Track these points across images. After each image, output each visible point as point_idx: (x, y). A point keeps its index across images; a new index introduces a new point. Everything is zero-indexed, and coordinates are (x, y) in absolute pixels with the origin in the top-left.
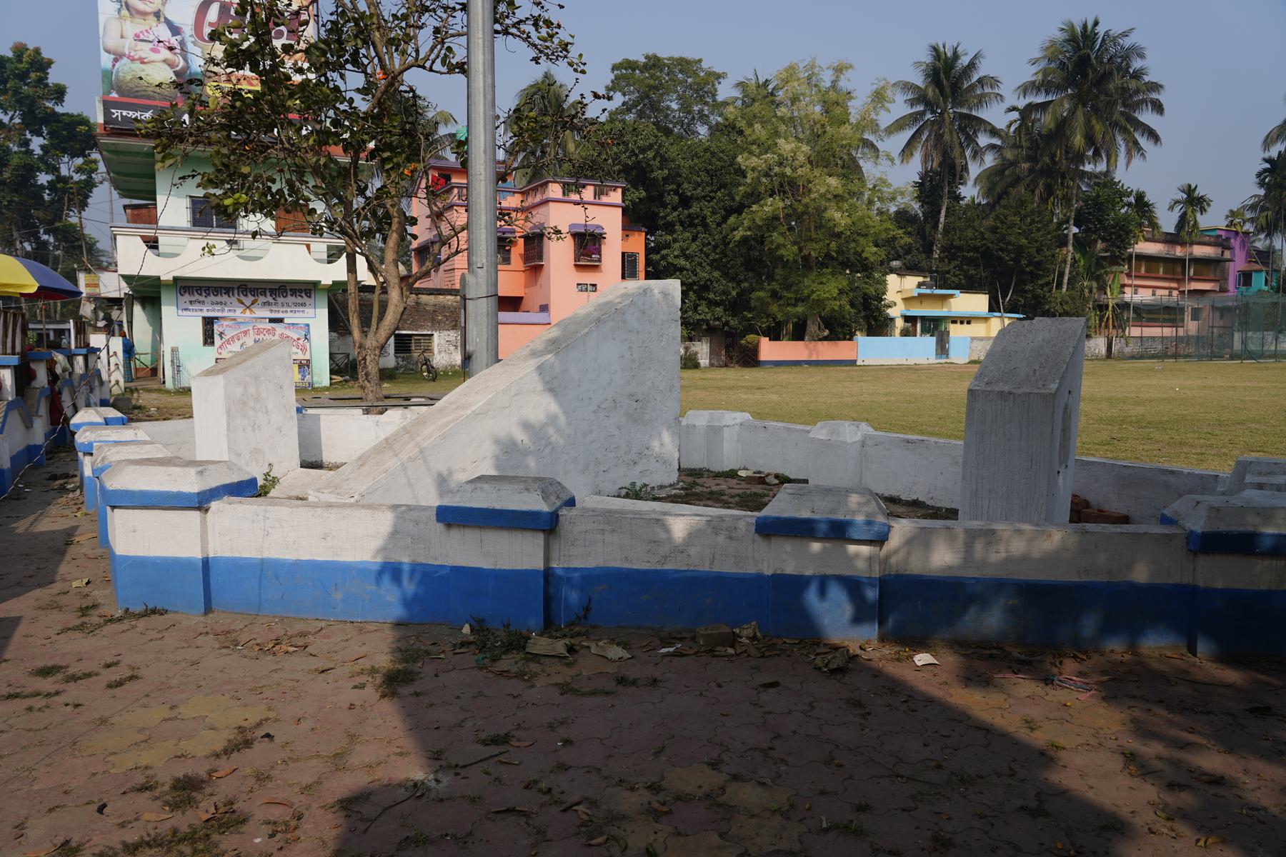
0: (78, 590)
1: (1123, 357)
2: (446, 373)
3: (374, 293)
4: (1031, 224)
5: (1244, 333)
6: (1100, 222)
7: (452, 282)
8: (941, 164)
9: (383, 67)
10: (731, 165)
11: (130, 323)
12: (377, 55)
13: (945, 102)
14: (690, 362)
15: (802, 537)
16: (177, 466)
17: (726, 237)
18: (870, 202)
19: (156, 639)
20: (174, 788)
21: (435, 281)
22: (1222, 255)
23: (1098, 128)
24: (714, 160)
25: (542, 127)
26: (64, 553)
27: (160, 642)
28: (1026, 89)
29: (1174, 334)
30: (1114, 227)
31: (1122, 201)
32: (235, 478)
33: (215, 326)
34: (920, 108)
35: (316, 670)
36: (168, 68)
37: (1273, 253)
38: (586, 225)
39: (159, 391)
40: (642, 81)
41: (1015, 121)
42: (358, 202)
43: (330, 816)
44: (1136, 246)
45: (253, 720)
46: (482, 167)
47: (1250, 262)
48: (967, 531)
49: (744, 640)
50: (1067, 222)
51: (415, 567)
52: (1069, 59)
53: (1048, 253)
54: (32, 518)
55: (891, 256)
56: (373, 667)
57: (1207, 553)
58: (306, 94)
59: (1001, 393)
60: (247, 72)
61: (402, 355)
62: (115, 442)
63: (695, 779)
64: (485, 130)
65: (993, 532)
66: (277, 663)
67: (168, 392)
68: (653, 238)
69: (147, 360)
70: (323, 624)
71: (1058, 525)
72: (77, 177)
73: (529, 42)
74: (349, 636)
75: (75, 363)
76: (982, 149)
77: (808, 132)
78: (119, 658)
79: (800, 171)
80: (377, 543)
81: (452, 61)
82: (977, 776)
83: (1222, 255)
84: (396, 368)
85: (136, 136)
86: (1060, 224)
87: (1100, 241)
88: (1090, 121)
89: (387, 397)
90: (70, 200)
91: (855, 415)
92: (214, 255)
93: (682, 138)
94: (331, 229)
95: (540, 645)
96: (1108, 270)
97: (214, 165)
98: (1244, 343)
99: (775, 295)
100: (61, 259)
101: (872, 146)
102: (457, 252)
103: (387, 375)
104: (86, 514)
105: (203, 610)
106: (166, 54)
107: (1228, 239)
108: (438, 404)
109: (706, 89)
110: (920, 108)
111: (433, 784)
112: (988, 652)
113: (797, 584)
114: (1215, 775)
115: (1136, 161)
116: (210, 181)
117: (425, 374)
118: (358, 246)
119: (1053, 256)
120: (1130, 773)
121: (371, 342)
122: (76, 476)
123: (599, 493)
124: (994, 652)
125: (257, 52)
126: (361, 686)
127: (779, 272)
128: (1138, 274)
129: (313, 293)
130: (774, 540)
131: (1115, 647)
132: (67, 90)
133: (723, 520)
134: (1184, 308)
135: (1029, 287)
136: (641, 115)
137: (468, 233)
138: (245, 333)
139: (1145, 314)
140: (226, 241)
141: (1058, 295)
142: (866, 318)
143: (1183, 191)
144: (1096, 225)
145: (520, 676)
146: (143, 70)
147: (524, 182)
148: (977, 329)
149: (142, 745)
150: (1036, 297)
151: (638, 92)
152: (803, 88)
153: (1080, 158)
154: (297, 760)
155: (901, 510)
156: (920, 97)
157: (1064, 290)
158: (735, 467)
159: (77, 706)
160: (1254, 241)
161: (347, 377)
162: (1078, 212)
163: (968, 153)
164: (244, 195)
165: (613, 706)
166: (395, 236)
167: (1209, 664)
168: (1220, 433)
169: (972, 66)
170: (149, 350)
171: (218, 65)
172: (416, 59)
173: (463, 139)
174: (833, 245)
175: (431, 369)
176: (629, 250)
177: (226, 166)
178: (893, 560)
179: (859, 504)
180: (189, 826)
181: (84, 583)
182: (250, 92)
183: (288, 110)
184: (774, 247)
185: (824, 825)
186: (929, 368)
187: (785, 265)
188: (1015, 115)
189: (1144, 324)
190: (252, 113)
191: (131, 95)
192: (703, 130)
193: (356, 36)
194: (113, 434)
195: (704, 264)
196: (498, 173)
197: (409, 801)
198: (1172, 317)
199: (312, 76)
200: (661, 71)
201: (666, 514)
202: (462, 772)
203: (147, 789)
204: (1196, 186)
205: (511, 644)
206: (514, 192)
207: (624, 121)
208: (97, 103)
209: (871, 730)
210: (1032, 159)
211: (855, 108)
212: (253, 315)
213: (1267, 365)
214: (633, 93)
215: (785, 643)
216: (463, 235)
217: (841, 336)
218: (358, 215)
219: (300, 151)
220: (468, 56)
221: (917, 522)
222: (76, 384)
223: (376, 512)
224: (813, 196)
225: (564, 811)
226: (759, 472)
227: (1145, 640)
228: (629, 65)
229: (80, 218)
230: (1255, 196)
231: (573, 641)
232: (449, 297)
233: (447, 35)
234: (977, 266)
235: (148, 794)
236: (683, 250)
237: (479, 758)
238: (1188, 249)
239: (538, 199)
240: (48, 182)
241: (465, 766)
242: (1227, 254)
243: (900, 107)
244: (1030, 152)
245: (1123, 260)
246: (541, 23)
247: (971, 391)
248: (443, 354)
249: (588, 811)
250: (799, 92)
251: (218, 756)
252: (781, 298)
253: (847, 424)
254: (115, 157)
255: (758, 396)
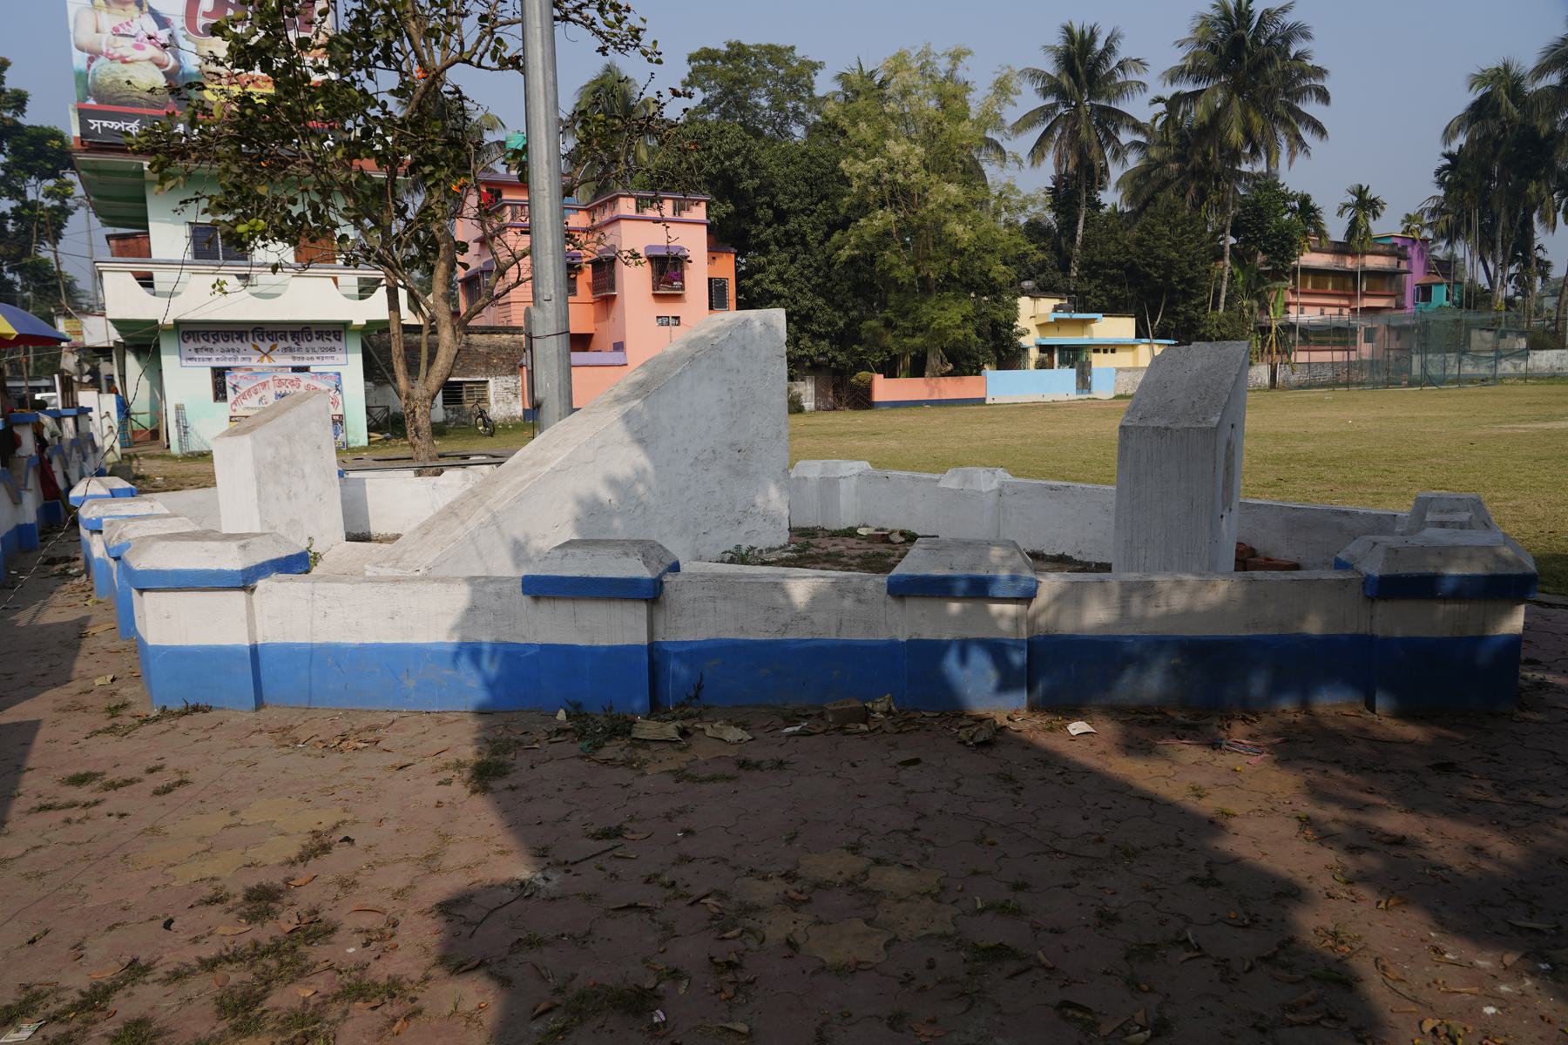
0: (102, 688)
1: (1288, 387)
2: (505, 426)
3: (421, 333)
4: (1182, 234)
5: (1423, 356)
6: (1260, 230)
7: (508, 319)
8: (1077, 167)
9: (421, 63)
10: (833, 172)
11: (123, 377)
12: (414, 48)
13: (1081, 91)
14: (795, 407)
15: (940, 597)
16: (214, 540)
17: (829, 257)
18: (997, 213)
19: (203, 740)
20: (248, 898)
21: (488, 317)
22: (1398, 266)
23: (1257, 121)
24: (813, 166)
25: (612, 132)
26: (78, 647)
27: (207, 742)
28: (1175, 75)
29: (1346, 359)
30: (1276, 236)
31: (1286, 206)
32: (282, 552)
33: (227, 378)
34: (1051, 100)
35: (393, 767)
36: (156, 68)
37: (1455, 262)
38: (668, 247)
39: (162, 457)
40: (724, 74)
41: (1161, 114)
42: (397, 226)
43: (429, 921)
44: (1301, 258)
45: (327, 824)
46: (546, 181)
47: (1429, 273)
48: (1123, 584)
49: (878, 715)
50: (1223, 231)
51: (496, 647)
52: (1222, 40)
53: (1202, 268)
54: (33, 609)
55: (1022, 276)
56: (458, 761)
57: (1386, 599)
58: (330, 97)
59: (1156, 429)
60: (257, 72)
61: (452, 406)
62: (129, 517)
63: (833, 865)
64: (547, 136)
65: (1152, 584)
66: (347, 760)
67: (174, 458)
68: (744, 261)
69: (145, 420)
70: (395, 716)
71: (1222, 574)
72: (48, 203)
73: (593, 29)
74: (426, 729)
75: (64, 425)
76: (1123, 147)
77: (922, 132)
78: (162, 762)
79: (914, 178)
80: (450, 621)
81: (503, 54)
82: (1142, 848)
83: (1398, 266)
84: (446, 422)
85: (125, 151)
86: (1215, 234)
87: (1260, 253)
88: (1247, 113)
89: (441, 456)
90: (39, 231)
91: (987, 462)
92: (226, 293)
93: (775, 140)
94: (368, 259)
95: (648, 729)
96: (1271, 286)
97: (223, 186)
98: (1424, 367)
99: (889, 324)
100: (32, 302)
101: (998, 148)
102: (519, 282)
103: (439, 430)
104: (98, 602)
105: (254, 705)
106: (151, 51)
107: (1404, 247)
108: (510, 462)
109: (800, 82)
110: (1051, 100)
111: (542, 883)
112: (1149, 717)
113: (936, 649)
114: (1394, 836)
115: (1300, 158)
116: (219, 205)
117: (480, 428)
118: (400, 278)
119: (1208, 271)
120: (1306, 838)
121: (420, 390)
122: (78, 559)
123: (700, 559)
124: (1156, 717)
125: (268, 49)
126: (448, 782)
127: (893, 298)
128: (1304, 290)
129: (343, 335)
130: (908, 601)
131: (1287, 705)
132: (29, 98)
133: (849, 582)
134: (1356, 329)
135: (1181, 308)
136: (725, 114)
137: (532, 260)
138: (264, 385)
139: (1313, 336)
140: (237, 275)
141: (1214, 317)
142: (996, 349)
143: (1354, 193)
145: (627, 763)
146: (126, 71)
147: (589, 197)
148: (1123, 359)
149: (204, 854)
150: (1189, 320)
151: (721, 86)
152: (917, 80)
153: (1235, 156)
154: (384, 864)
155: (1046, 566)
156: (1051, 87)
157: (1221, 310)
158: (855, 525)
159: (122, 816)
160: (1433, 249)
161: (388, 435)
162: (1236, 219)
163: (1108, 152)
164: (261, 221)
165: (735, 792)
166: (443, 265)
167: (1389, 720)
168: (1396, 469)
169: (1109, 48)
170: (147, 408)
171: (222, 64)
172: (461, 53)
173: (520, 147)
174: (955, 264)
175: (487, 422)
176: (717, 275)
177: (238, 188)
178: (1042, 620)
179: (1002, 558)
180: (271, 938)
181: (109, 680)
182: (262, 97)
183: (309, 117)
184: (886, 268)
185: (979, 906)
186: (1068, 405)
187: (900, 288)
188: (1161, 107)
189: (1312, 348)
190: (265, 123)
191: (113, 102)
192: (798, 131)
193: (387, 27)
194: (125, 507)
195: (805, 290)
196: (564, 188)
197: (515, 903)
198: (1343, 339)
199: (333, 76)
200: (747, 61)
201: (784, 576)
202: (574, 869)
203: (217, 901)
204: (1368, 188)
205: (615, 730)
206: (578, 210)
207: (705, 122)
208: (71, 113)
209: (1024, 806)
210: (1181, 158)
211: (976, 102)
212: (273, 364)
213: (1449, 391)
214: (714, 88)
215: (924, 716)
216: (525, 262)
217: (967, 370)
218: (399, 241)
219: (326, 166)
220: (523, 48)
221: (1068, 576)
222: (66, 451)
223: (452, 586)
224: (930, 207)
225: (692, 904)
226: (882, 530)
227: (1319, 697)
228: (708, 55)
229: (55, 252)
230: (1434, 197)
231: (685, 724)
232: (505, 336)
234: (1122, 285)
235: (218, 906)
236: (780, 274)
237: (590, 854)
238: (1360, 260)
239: (607, 216)
240: (12, 209)
241: (576, 863)
242: (1404, 266)
243: (1030, 99)
244: (1178, 150)
245: (1287, 275)
246: (607, 7)
247: (1122, 427)
248: (501, 404)
249: (718, 904)
250: (910, 84)
251: (293, 863)
252: (895, 328)
253: (981, 470)
254: (95, 177)
255: (874, 443)
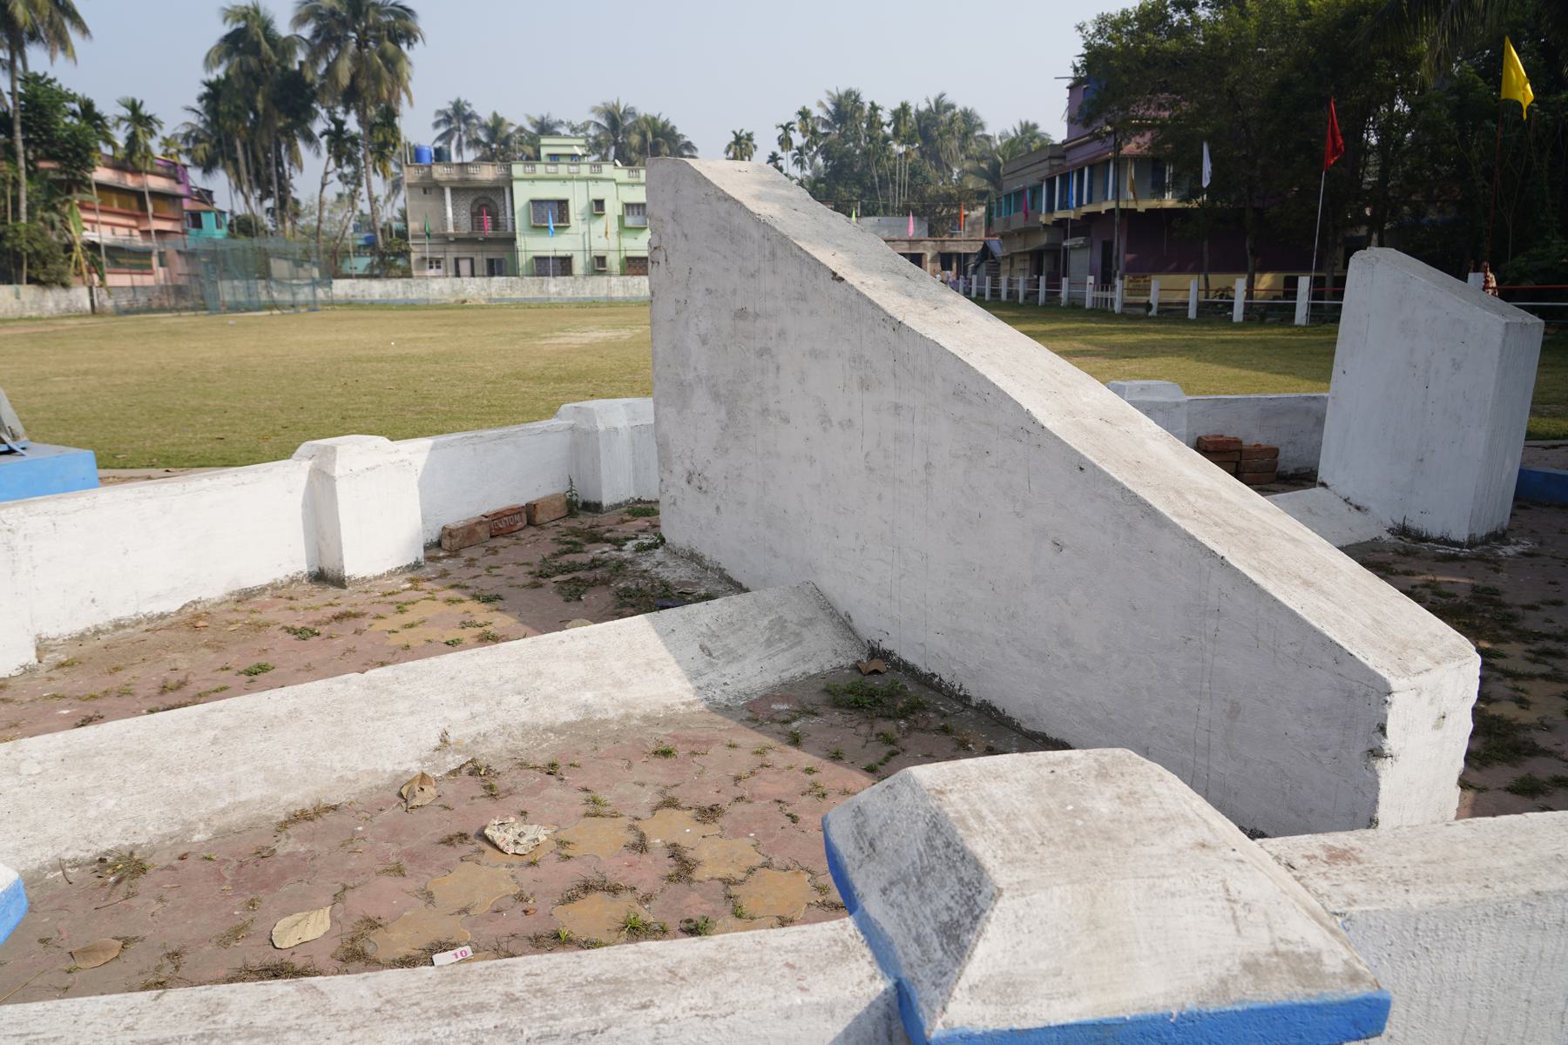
143: (126, 106)
144: (40, 136)
230: (188, 123)
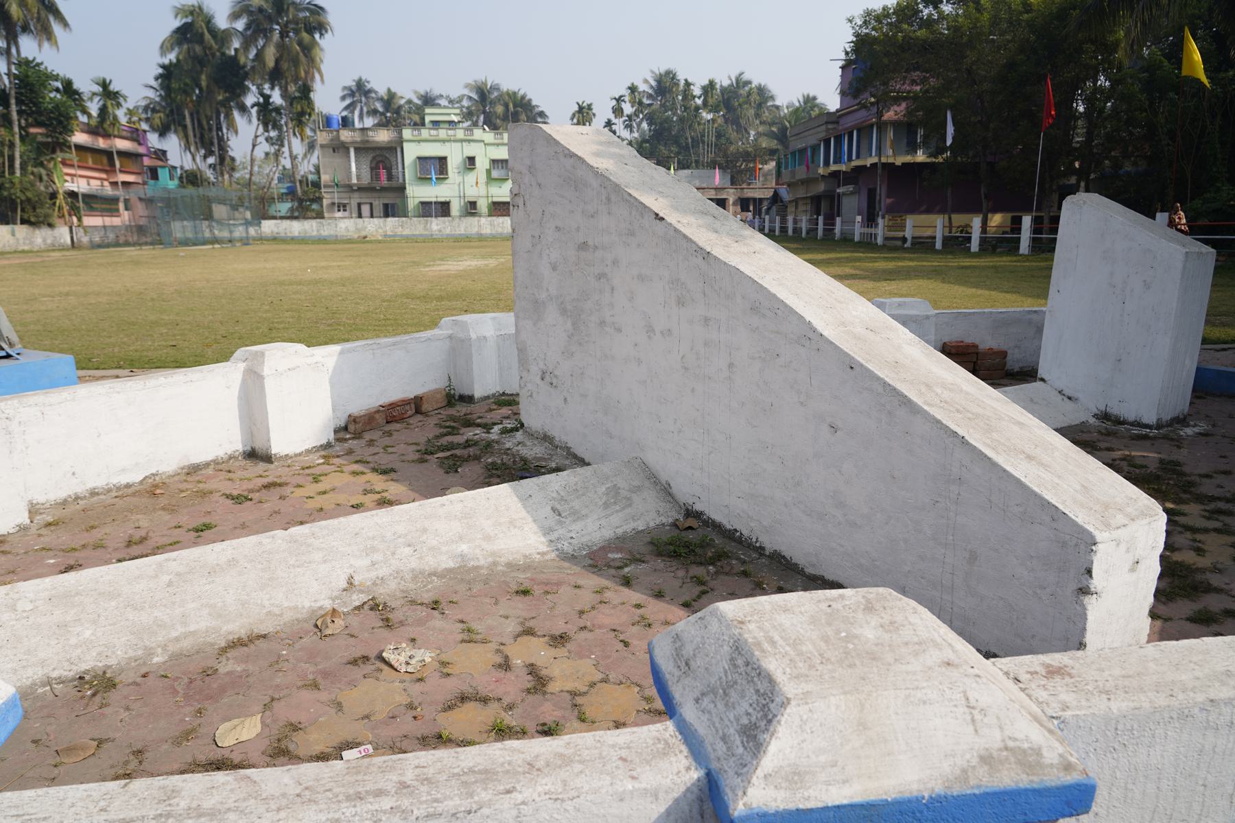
143: (98, 84)
144: (30, 107)
233: (247, 238)
238: (109, 142)
